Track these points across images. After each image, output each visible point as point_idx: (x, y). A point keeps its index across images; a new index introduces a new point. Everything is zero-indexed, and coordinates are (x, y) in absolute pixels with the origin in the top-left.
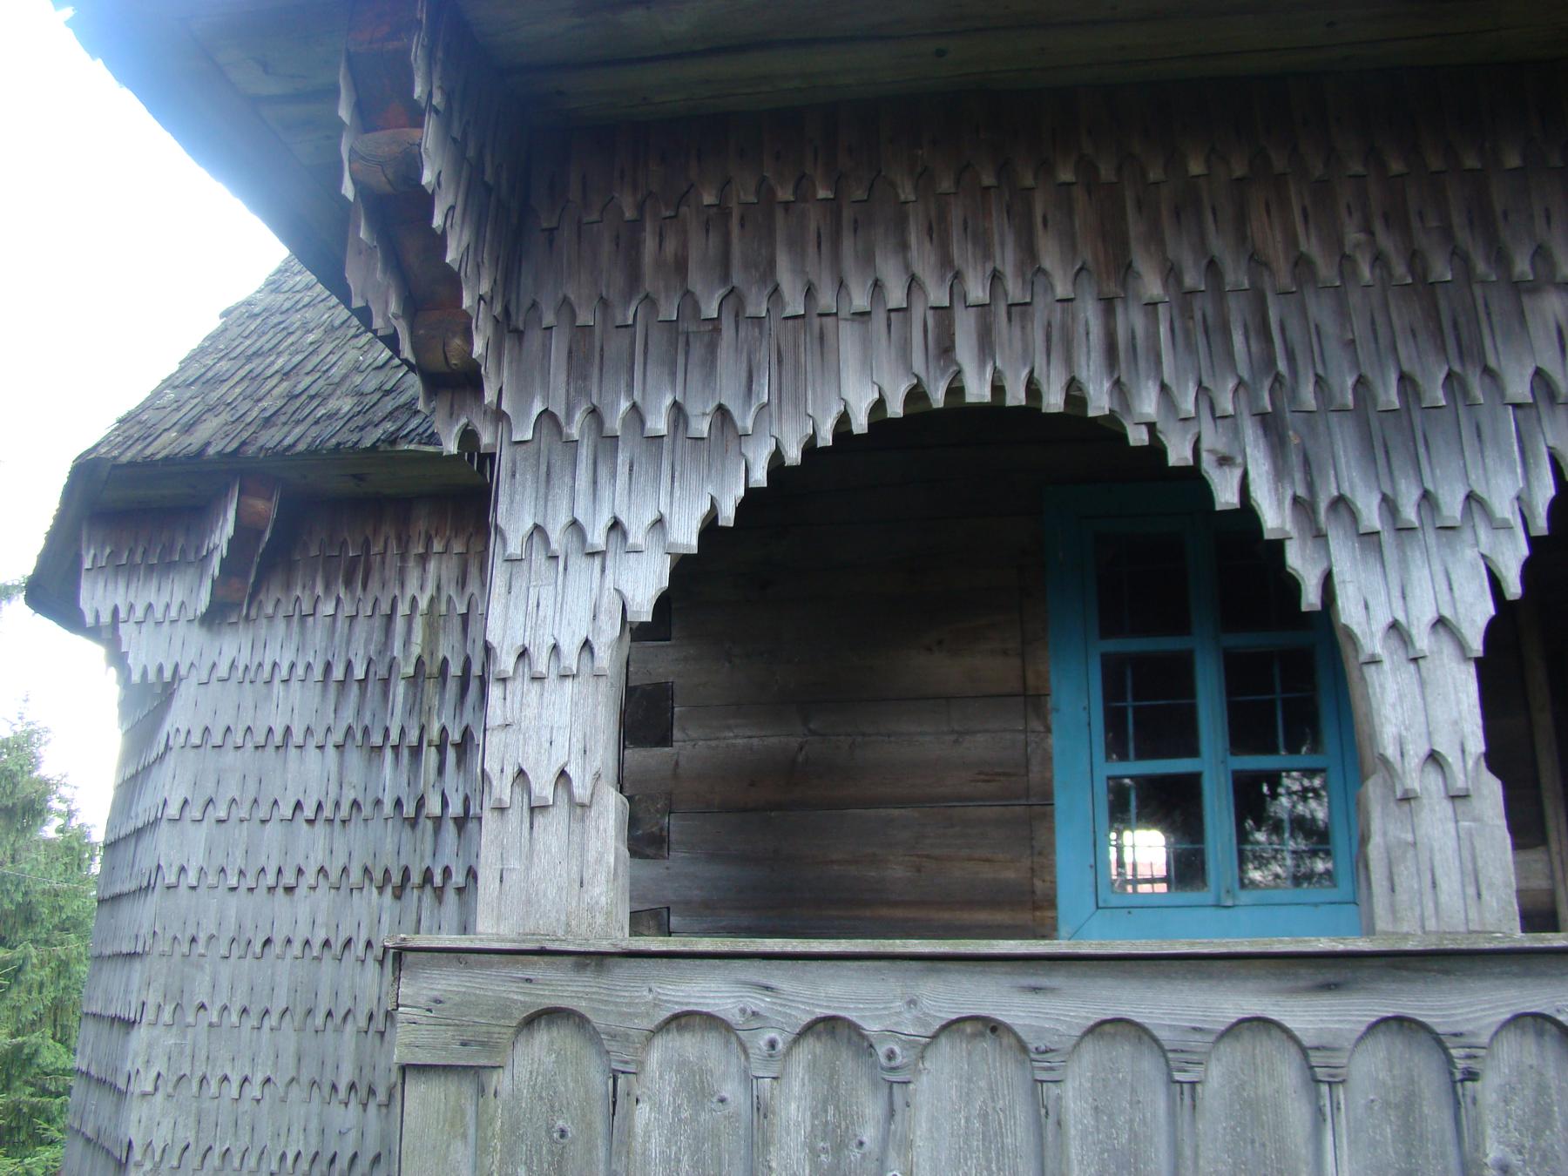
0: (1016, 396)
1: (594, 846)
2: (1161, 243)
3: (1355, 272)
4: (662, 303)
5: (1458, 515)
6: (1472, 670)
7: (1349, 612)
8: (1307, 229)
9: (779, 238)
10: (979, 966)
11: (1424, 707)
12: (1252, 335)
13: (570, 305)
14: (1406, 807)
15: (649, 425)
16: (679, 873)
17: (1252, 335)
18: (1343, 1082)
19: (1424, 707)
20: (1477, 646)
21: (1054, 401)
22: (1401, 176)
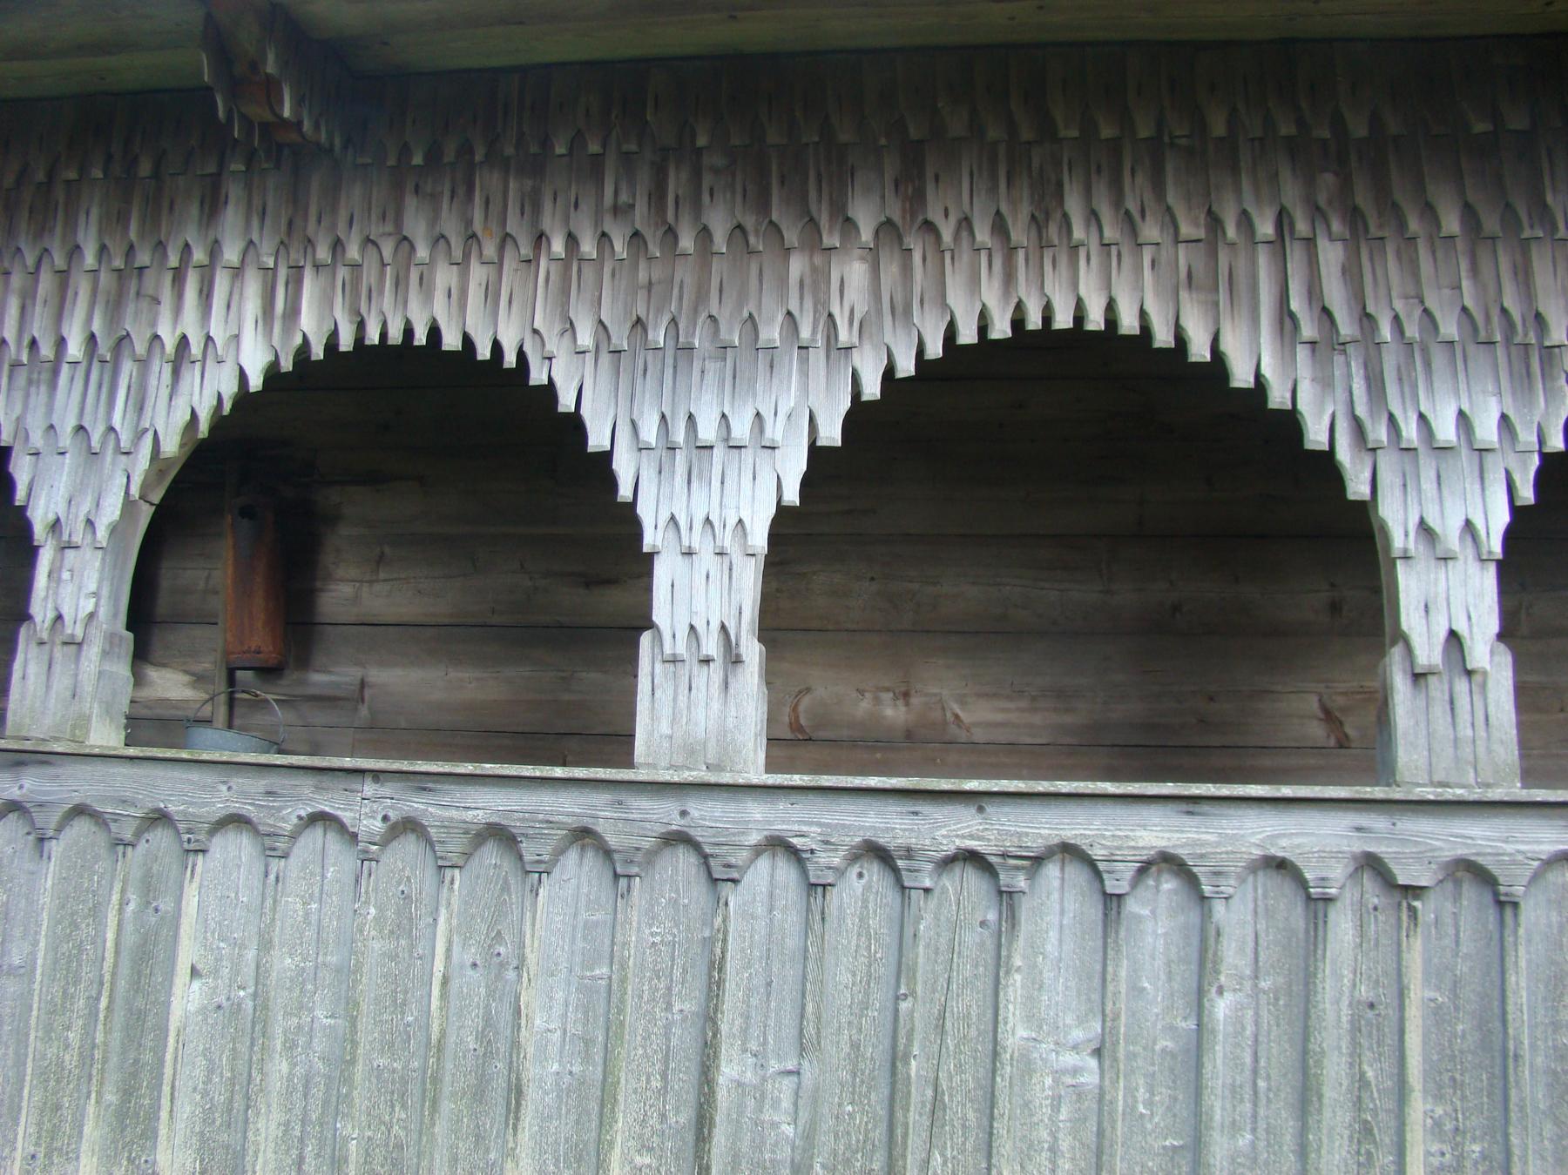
0: (1063, 320)
1: (84, 663)
2: (537, 210)
3: (165, 256)
4: (1257, 221)
5: (1495, 438)
6: (1492, 570)
7: (645, 511)
8: (820, 195)
9: (1242, 164)
10: (169, 765)
11: (1447, 597)
12: (101, 299)
13: (374, 243)
14: (671, 667)
15: (1442, 330)
16: (1298, 709)
17: (101, 299)
18: (204, 851)
19: (1447, 597)
20: (1496, 546)
21: (420, 338)
22: (1029, 143)
